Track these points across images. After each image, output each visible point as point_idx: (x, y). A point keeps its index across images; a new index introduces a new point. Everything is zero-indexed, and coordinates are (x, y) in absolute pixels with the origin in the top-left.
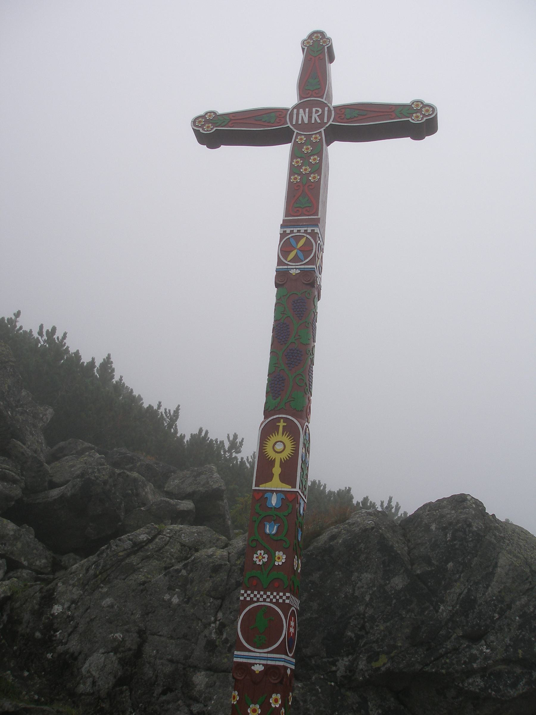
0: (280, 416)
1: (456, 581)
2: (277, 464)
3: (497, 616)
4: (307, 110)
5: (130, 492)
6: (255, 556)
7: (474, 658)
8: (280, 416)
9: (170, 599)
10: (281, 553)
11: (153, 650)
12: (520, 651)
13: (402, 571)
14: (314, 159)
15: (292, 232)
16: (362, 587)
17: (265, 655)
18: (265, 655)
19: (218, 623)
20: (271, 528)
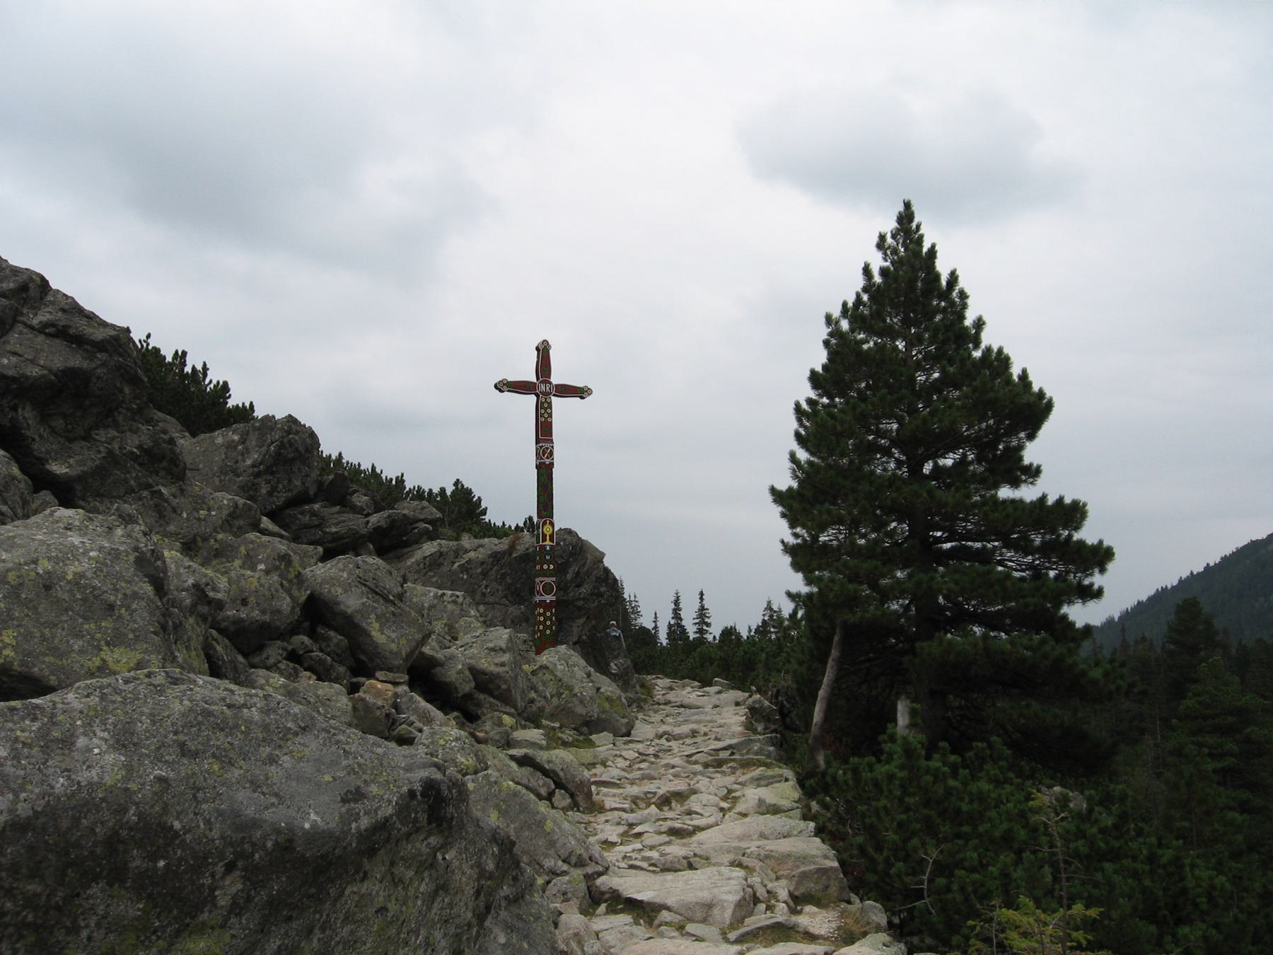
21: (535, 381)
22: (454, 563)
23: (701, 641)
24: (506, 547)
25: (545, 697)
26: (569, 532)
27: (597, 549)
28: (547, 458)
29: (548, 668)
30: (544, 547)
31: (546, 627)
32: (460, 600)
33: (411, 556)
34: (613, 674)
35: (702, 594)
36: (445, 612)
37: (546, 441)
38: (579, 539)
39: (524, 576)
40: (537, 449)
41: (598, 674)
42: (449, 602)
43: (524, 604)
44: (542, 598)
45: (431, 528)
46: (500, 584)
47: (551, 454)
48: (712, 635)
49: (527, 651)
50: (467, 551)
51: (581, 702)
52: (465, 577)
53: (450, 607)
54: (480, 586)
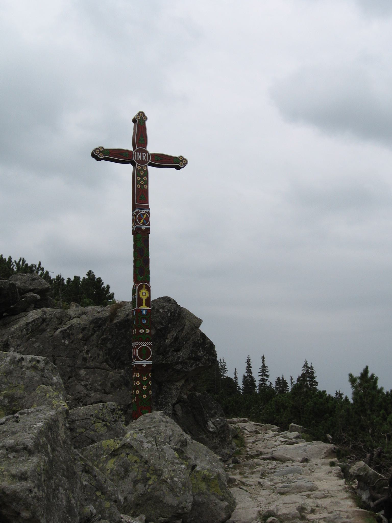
0: (144, 283)
3: (184, 343)
4: (140, 153)
5: (14, 291)
6: (140, 330)
7: (179, 358)
8: (144, 283)
9: (64, 342)
10: (148, 329)
11: (60, 363)
12: (193, 355)
13: (154, 328)
15: (141, 211)
19: (85, 350)
20: (144, 321)
21: (131, 149)
22: (57, 329)
23: (263, 387)
24: (108, 314)
25: (115, 501)
26: (168, 300)
27: (194, 317)
28: (143, 223)
29: (132, 447)
30: (140, 311)
31: (142, 392)
32: (41, 365)
33: (17, 323)
34: (210, 432)
35: (263, 358)
36: (22, 379)
37: (141, 207)
38: (178, 306)
39: (124, 341)
40: (133, 215)
41: (194, 441)
42: (28, 368)
43: (124, 369)
44: (138, 363)
45: (39, 297)
46: (101, 349)
47: (147, 220)
48: (270, 382)
49: (115, 421)
50: (71, 318)
51: (172, 490)
52: (67, 342)
53: (28, 373)
54: (81, 352)
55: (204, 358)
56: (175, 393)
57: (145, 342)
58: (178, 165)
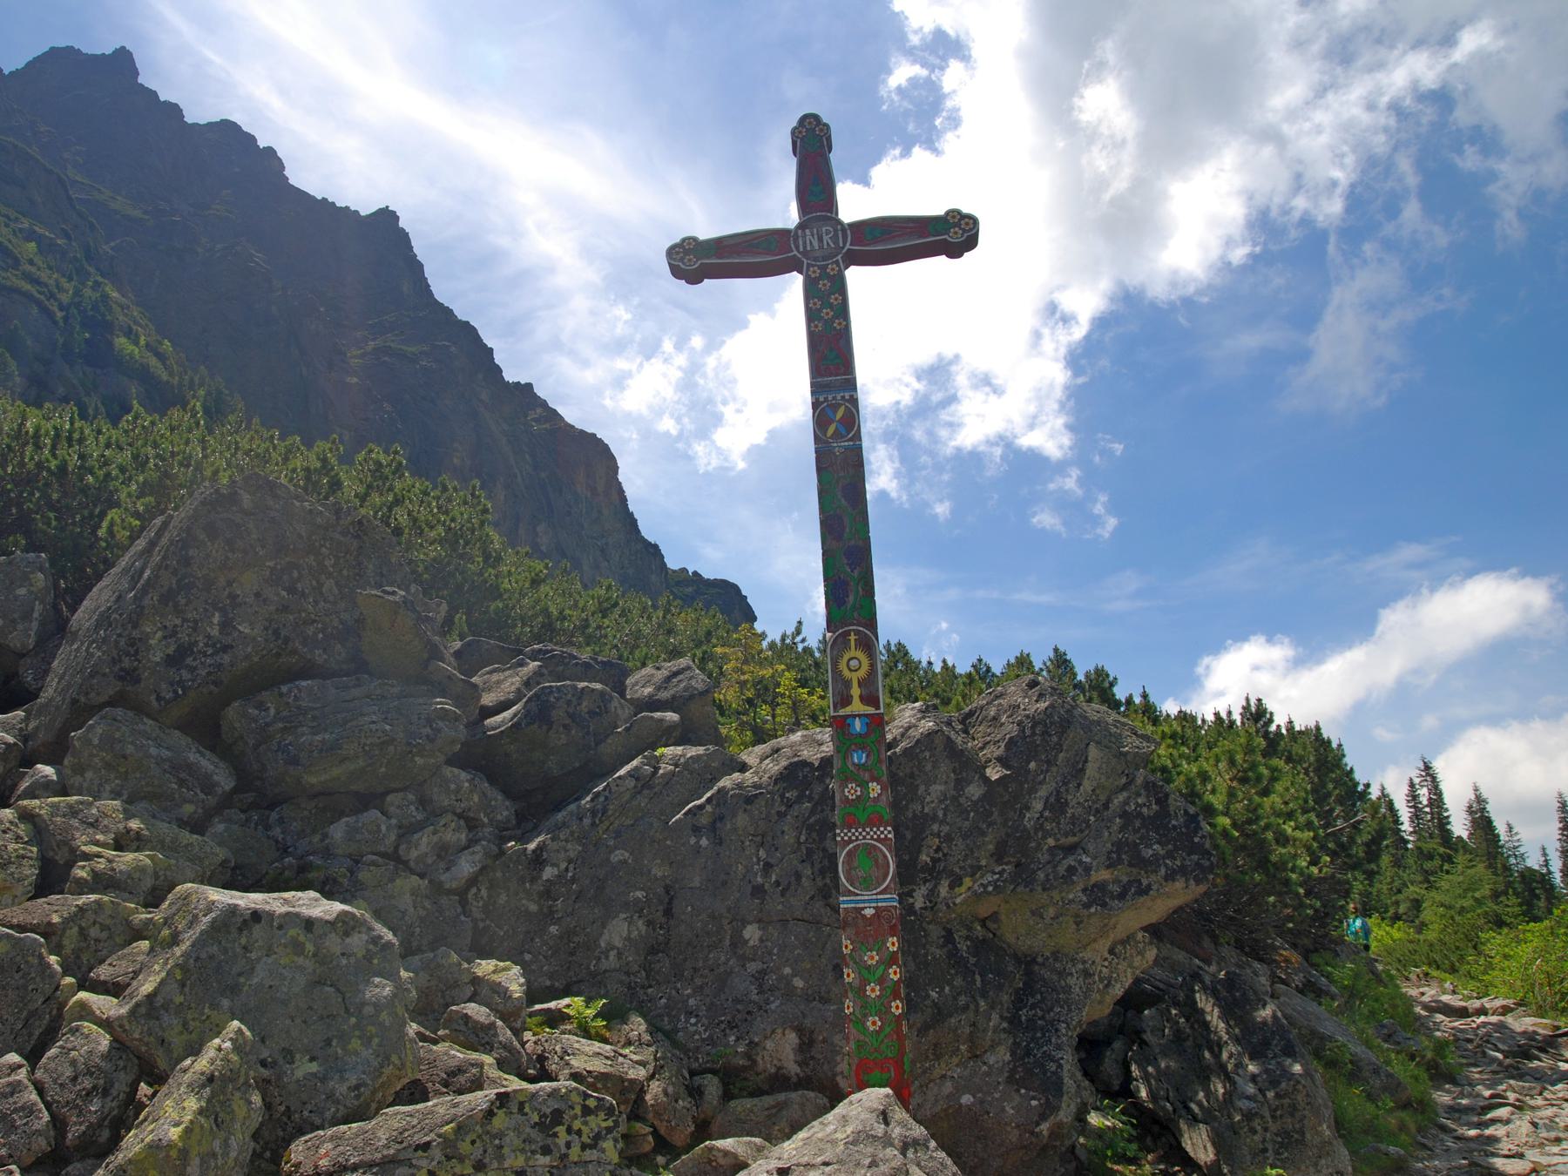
1: (1040, 783)
2: (855, 684)
10: (875, 784)
13: (976, 778)
14: (836, 299)
16: (932, 802)
17: (874, 897)
18: (874, 897)
55: (1166, 865)
56: (1081, 988)
57: (868, 830)
58: (945, 239)
